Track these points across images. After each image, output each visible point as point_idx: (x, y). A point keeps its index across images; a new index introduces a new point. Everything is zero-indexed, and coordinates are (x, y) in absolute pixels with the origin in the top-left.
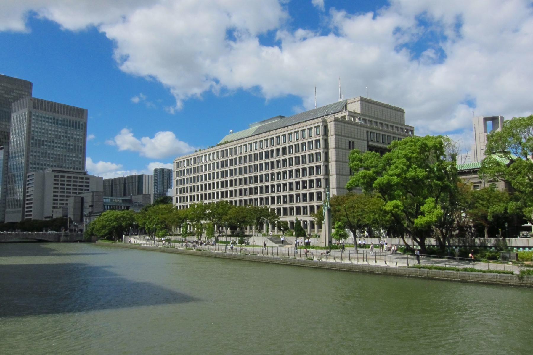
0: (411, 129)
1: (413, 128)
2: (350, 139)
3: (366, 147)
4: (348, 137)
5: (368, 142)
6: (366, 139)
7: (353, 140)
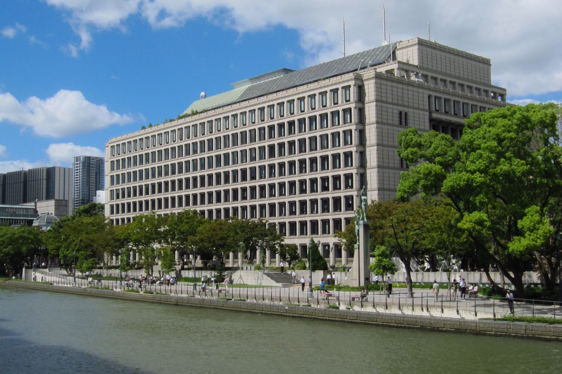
0: (502, 92)
1: (505, 90)
2: (401, 109)
3: (427, 121)
4: (398, 105)
5: (430, 113)
6: (427, 108)
7: (406, 110)
